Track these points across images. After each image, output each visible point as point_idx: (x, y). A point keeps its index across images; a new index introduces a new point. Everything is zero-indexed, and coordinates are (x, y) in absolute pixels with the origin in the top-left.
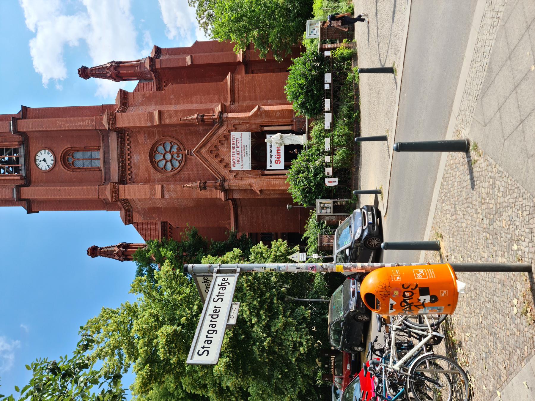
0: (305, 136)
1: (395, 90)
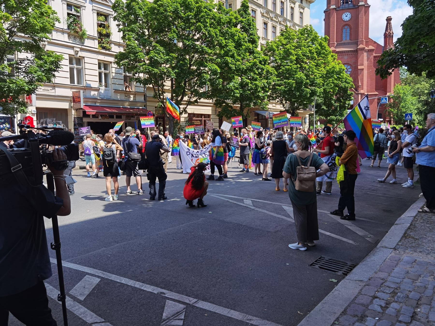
1: (256, 142)
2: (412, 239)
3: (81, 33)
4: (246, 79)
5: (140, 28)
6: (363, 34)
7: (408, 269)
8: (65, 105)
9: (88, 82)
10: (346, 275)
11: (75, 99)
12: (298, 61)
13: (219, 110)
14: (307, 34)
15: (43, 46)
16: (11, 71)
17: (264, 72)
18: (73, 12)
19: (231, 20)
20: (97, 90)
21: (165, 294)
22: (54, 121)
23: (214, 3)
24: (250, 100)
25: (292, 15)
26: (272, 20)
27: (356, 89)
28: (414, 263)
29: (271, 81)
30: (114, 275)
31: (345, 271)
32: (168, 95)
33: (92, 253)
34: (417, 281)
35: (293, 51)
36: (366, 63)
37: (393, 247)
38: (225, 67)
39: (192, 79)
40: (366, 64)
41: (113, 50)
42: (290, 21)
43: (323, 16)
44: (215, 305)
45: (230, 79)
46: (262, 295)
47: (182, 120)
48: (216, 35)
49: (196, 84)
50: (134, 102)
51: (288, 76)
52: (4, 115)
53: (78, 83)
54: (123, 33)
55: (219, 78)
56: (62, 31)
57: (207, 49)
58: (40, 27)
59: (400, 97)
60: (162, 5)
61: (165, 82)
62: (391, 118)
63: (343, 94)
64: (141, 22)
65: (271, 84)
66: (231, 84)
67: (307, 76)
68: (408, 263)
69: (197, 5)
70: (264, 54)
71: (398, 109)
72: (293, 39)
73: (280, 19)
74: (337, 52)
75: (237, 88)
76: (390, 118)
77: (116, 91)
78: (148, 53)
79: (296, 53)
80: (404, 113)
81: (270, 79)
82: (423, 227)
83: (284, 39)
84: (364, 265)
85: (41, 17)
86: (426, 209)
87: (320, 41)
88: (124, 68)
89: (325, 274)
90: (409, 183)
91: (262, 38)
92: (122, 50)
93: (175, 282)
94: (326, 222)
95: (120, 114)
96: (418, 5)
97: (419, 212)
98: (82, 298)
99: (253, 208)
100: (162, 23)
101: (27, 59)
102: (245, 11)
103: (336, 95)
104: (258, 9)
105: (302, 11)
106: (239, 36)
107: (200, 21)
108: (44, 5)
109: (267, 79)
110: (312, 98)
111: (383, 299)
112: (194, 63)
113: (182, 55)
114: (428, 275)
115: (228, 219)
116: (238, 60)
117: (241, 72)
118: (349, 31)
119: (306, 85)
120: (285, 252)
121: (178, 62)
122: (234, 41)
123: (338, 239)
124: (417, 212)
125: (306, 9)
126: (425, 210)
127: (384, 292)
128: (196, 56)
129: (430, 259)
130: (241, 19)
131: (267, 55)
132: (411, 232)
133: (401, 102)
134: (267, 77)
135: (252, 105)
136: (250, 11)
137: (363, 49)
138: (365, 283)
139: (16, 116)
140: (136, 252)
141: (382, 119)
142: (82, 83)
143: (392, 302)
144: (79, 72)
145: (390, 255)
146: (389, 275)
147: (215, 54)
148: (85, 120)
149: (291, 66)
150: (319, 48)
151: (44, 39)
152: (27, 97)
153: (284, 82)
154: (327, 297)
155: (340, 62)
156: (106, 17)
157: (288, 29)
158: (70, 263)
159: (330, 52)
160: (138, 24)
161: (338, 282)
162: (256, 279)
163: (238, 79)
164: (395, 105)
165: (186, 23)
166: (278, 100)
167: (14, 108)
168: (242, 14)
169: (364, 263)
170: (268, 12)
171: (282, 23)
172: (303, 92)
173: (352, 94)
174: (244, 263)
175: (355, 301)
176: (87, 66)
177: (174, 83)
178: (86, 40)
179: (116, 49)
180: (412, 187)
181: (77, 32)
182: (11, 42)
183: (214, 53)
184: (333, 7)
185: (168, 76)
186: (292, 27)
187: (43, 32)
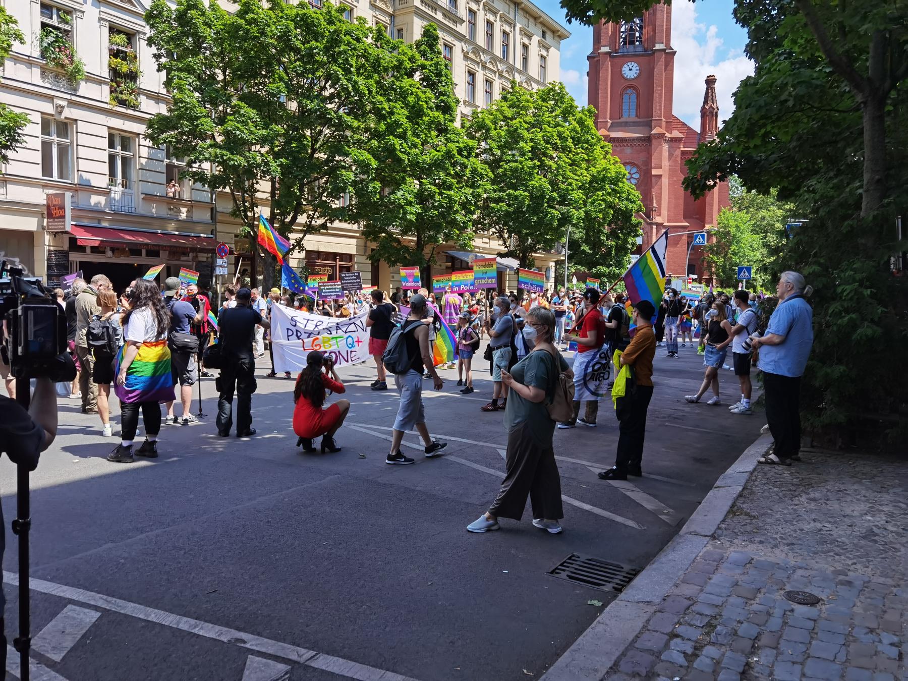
3: (71, 68)
4: (431, 184)
5: (205, 64)
6: (661, 106)
7: (737, 577)
8: (29, 224)
10: (620, 591)
11: (53, 211)
12: (536, 153)
13: (374, 245)
17: (467, 172)
18: (55, 21)
19: (401, 63)
20: (106, 193)
21: (245, 642)
23: (367, 26)
24: (438, 228)
25: (525, 59)
26: (484, 67)
27: (648, 215)
29: (480, 190)
31: (617, 584)
32: (264, 212)
34: (753, 602)
36: (666, 163)
37: (710, 534)
39: (316, 179)
40: (666, 167)
42: (520, 72)
44: (354, 663)
48: (370, 92)
50: (189, 221)
51: (514, 181)
53: (61, 175)
54: (168, 74)
55: (374, 180)
57: (348, 119)
59: (729, 233)
60: (255, 21)
61: (257, 183)
62: (712, 273)
63: (623, 222)
65: (480, 196)
66: (400, 194)
68: (737, 564)
70: (467, 136)
72: (526, 109)
73: (501, 67)
75: (411, 202)
78: (221, 121)
79: (530, 136)
80: (736, 265)
81: (478, 187)
82: (766, 494)
87: (578, 116)
89: (580, 589)
91: (465, 102)
92: (163, 110)
93: (269, 616)
95: (157, 248)
97: (760, 462)
98: (57, 657)
102: (431, 47)
105: (544, 53)
106: (417, 95)
107: (335, 61)
109: (472, 186)
111: (689, 640)
112: (322, 146)
113: (297, 129)
114: (775, 588)
117: (419, 170)
121: (288, 143)
122: (407, 105)
123: (607, 519)
124: (756, 463)
128: (327, 131)
129: (779, 556)
130: (421, 61)
131: (472, 137)
133: (731, 244)
134: (473, 183)
136: (440, 47)
137: (661, 137)
141: (695, 277)
142: (70, 177)
143: (705, 645)
144: (63, 151)
145: (705, 549)
146: (702, 590)
147: (367, 130)
148: (75, 257)
149: (521, 163)
150: (579, 129)
154: (581, 637)
155: (617, 159)
156: (131, 36)
157: (517, 88)
160: (201, 57)
163: (414, 185)
165: (305, 63)
166: (494, 230)
168: (425, 51)
169: (654, 566)
170: (477, 50)
177: (277, 185)
178: (83, 83)
180: (749, 412)
181: (63, 66)
185: (265, 173)
186: (524, 85)
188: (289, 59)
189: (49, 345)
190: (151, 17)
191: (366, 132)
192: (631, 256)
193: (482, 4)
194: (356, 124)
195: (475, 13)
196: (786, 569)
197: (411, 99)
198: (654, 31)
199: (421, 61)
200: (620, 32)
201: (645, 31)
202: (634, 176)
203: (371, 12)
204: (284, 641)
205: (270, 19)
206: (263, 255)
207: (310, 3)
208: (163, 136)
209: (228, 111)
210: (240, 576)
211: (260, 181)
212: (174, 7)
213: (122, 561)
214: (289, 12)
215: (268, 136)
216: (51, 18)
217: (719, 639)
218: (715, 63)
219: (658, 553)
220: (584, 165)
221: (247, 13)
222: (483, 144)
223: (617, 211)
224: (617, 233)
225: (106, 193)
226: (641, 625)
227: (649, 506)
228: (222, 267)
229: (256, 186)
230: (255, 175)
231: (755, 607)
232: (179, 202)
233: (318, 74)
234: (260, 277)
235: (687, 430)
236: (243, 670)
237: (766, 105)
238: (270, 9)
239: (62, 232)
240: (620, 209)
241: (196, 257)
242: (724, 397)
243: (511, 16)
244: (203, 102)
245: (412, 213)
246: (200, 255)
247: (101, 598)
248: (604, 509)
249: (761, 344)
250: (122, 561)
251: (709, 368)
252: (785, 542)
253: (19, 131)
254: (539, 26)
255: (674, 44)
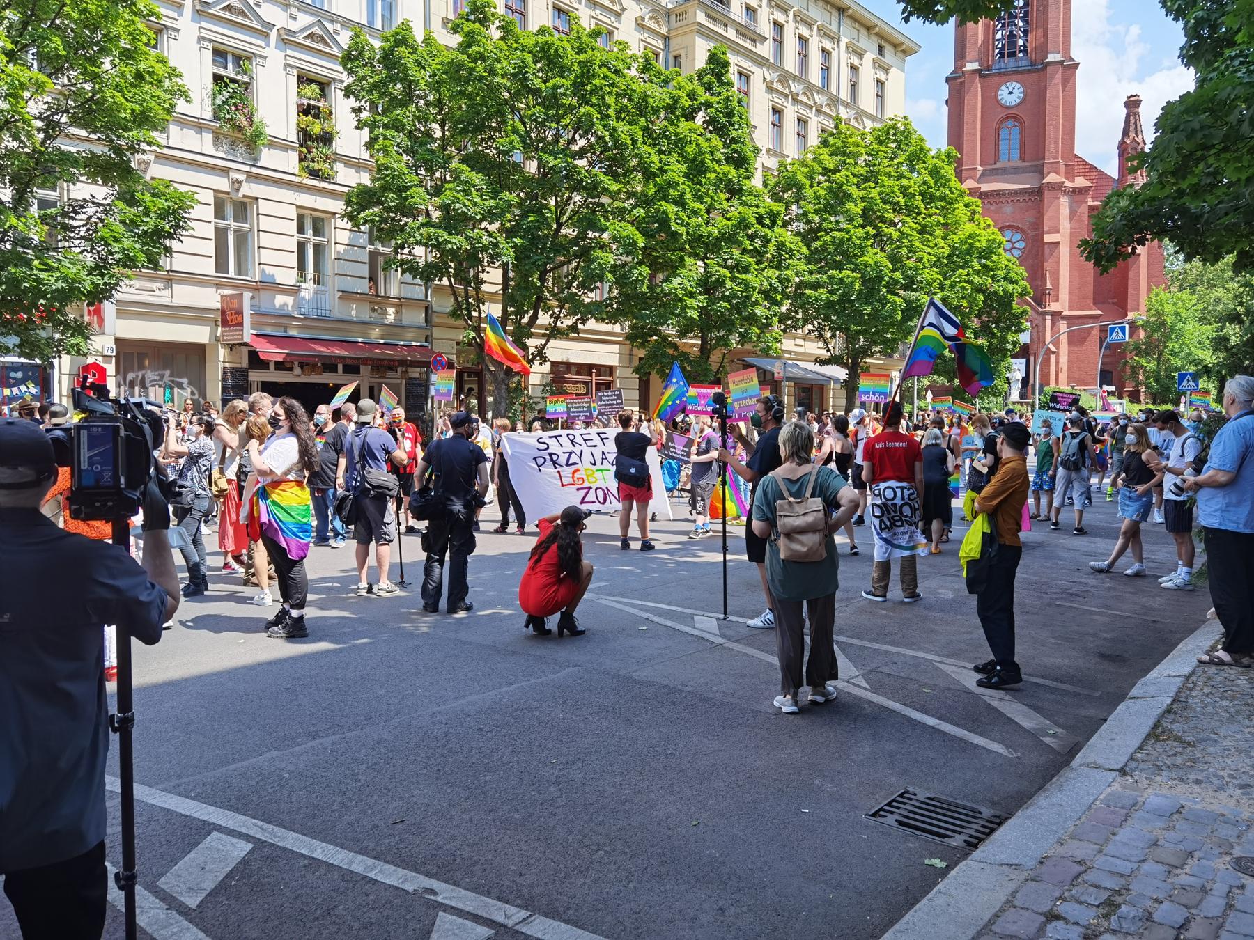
0: (1018, 399)
2: (1175, 744)
3: (249, 131)
4: (719, 265)
5: (418, 118)
6: (1057, 143)
7: (1158, 833)
8: (198, 334)
9: (269, 270)
10: (975, 846)
11: (229, 317)
12: (868, 216)
13: (642, 353)
14: (895, 141)
15: (143, 166)
16: (50, 235)
17: (771, 248)
18: (230, 72)
19: (676, 100)
20: (294, 291)
21: (435, 893)
22: (166, 379)
23: (630, 53)
24: (729, 325)
25: (854, 86)
26: (795, 101)
27: (1039, 300)
28: (1176, 816)
29: (789, 272)
30: (294, 835)
31: (971, 836)
32: (494, 310)
33: (238, 765)
34: (1179, 871)
35: (854, 191)
36: (1065, 225)
37: (1118, 767)
38: (659, 230)
39: (563, 264)
40: (1064, 228)
41: (340, 178)
42: (846, 105)
43: (944, 91)
44: (580, 931)
45: (672, 267)
46: (720, 904)
47: (534, 379)
48: (634, 142)
49: (574, 278)
50: (399, 326)
51: (838, 258)
52: (22, 360)
53: (239, 272)
54: (371, 132)
55: (640, 263)
56: (199, 126)
57: (607, 181)
58: (133, 111)
59: (1164, 324)
60: (482, 57)
61: (483, 271)
62: (1138, 383)
63: (999, 311)
64: (422, 102)
65: (789, 281)
66: (676, 282)
67: (895, 259)
68: (1158, 813)
69: (583, 57)
70: (771, 197)
71: (1158, 359)
72: (855, 156)
73: (820, 99)
74: (983, 195)
75: (691, 293)
76: (1137, 386)
77: (347, 295)
78: (438, 191)
79: (862, 194)
80: (1177, 369)
81: (787, 268)
82: (1209, 709)
83: (831, 155)
84: (1029, 817)
85: (135, 86)
86: (1221, 654)
87: (931, 161)
88: (371, 230)
89: (915, 842)
90: (1177, 577)
91: (768, 151)
92: (365, 179)
93: (471, 858)
94: (929, 686)
95: (356, 362)
96: (1209, 63)
97: (1201, 662)
98: (192, 901)
99: (719, 640)
100: (481, 105)
101: (94, 203)
102: (718, 77)
103: (978, 316)
104: (755, 69)
105: (881, 76)
106: (698, 145)
107: (587, 103)
108: (145, 53)
109: (778, 267)
110: (910, 323)
111: (1077, 924)
112: (570, 218)
113: (535, 197)
114: (1216, 851)
115: (643, 674)
116: (695, 213)
117: (706, 246)
118: (1018, 136)
119: (892, 286)
120: (800, 774)
121: (524, 215)
122: (684, 157)
123: (961, 740)
124: (1195, 663)
125: (893, 71)
126: (1218, 658)
127: (1081, 903)
128: (577, 198)
129: (1226, 803)
130: (705, 97)
131: (779, 199)
132: (1174, 722)
133: (1169, 338)
134: (780, 262)
135: (734, 340)
136: (732, 75)
137: (1058, 187)
138: (1026, 874)
139: (56, 362)
140: (364, 767)
141: (1113, 388)
142: (250, 273)
143: (1101, 933)
144: (242, 239)
145: (1109, 790)
146: (1100, 851)
147: (630, 195)
148: (255, 376)
149: (848, 232)
150: (931, 181)
151: (144, 146)
152: (92, 308)
153: (829, 277)
154: (912, 912)
155: (989, 221)
156: (324, 86)
157: (843, 127)
158: (169, 795)
159: (962, 194)
160: (413, 108)
161: (949, 868)
162: (709, 855)
163: (695, 268)
164: (1151, 348)
165: (546, 108)
166: (810, 327)
167: (52, 338)
168: (710, 84)
169: (1029, 812)
170: (785, 77)
171: (826, 109)
172: (884, 305)
173: (1025, 312)
174: (679, 806)
175: (994, 928)
176: (265, 223)
177: (511, 274)
178: (265, 150)
179: (349, 178)
180: (1190, 588)
181: (240, 129)
182: (49, 154)
183: (627, 192)
184: (972, 66)
185: (494, 258)
186: (853, 122)
187: (139, 126)
188: (527, 105)
189: (107, 476)
190: (349, 59)
191: (628, 198)
192: (1013, 360)
193: (791, 13)
194: (615, 187)
195: (782, 26)
196: (1236, 823)
197: (690, 150)
198: (1046, 35)
199: (705, 97)
200: (994, 40)
201: (1031, 37)
202: (1016, 245)
203: (638, 35)
204: (488, 894)
205: (501, 51)
206: (492, 368)
207: (555, 28)
208: (362, 215)
209: (448, 177)
210: (436, 802)
211: (487, 269)
212: (377, 44)
213: (287, 775)
214: (525, 42)
215: (496, 208)
216: (226, 67)
217: (1124, 924)
218: (1140, 79)
219: (1036, 793)
220: (939, 232)
221: (470, 46)
222: (794, 208)
223: (990, 296)
224: (990, 328)
225: (294, 291)
226: (1003, 899)
227: (1025, 724)
228: (442, 383)
229: (481, 275)
230: (480, 262)
231: (1184, 879)
232: (385, 300)
233: (563, 122)
234: (490, 399)
235: (1091, 613)
236: (430, 932)
237: (1202, 128)
238: (501, 39)
239: (240, 344)
240: (995, 293)
241: (407, 372)
242: (1152, 565)
243: (834, 27)
244: (414, 168)
245: (693, 308)
246: (410, 369)
247: (255, 825)
248: (956, 725)
249: (1198, 486)
250: (287, 775)
251: (1127, 521)
252: (1235, 781)
253: (186, 215)
254: (875, 38)
255: (1075, 53)
